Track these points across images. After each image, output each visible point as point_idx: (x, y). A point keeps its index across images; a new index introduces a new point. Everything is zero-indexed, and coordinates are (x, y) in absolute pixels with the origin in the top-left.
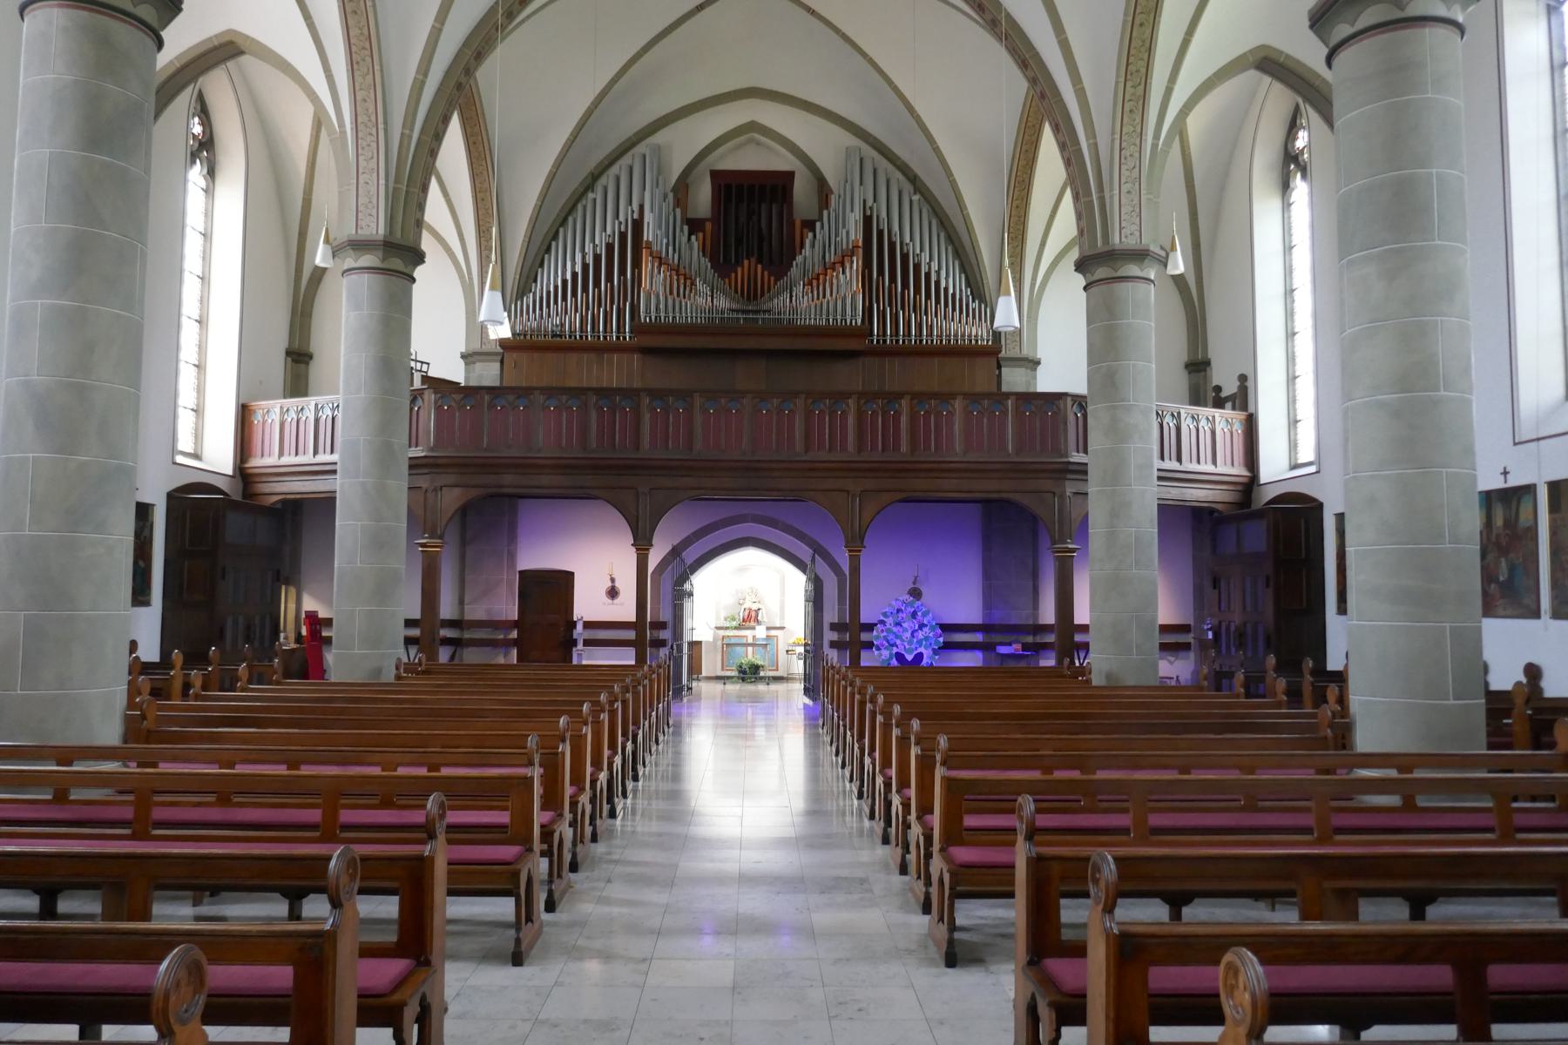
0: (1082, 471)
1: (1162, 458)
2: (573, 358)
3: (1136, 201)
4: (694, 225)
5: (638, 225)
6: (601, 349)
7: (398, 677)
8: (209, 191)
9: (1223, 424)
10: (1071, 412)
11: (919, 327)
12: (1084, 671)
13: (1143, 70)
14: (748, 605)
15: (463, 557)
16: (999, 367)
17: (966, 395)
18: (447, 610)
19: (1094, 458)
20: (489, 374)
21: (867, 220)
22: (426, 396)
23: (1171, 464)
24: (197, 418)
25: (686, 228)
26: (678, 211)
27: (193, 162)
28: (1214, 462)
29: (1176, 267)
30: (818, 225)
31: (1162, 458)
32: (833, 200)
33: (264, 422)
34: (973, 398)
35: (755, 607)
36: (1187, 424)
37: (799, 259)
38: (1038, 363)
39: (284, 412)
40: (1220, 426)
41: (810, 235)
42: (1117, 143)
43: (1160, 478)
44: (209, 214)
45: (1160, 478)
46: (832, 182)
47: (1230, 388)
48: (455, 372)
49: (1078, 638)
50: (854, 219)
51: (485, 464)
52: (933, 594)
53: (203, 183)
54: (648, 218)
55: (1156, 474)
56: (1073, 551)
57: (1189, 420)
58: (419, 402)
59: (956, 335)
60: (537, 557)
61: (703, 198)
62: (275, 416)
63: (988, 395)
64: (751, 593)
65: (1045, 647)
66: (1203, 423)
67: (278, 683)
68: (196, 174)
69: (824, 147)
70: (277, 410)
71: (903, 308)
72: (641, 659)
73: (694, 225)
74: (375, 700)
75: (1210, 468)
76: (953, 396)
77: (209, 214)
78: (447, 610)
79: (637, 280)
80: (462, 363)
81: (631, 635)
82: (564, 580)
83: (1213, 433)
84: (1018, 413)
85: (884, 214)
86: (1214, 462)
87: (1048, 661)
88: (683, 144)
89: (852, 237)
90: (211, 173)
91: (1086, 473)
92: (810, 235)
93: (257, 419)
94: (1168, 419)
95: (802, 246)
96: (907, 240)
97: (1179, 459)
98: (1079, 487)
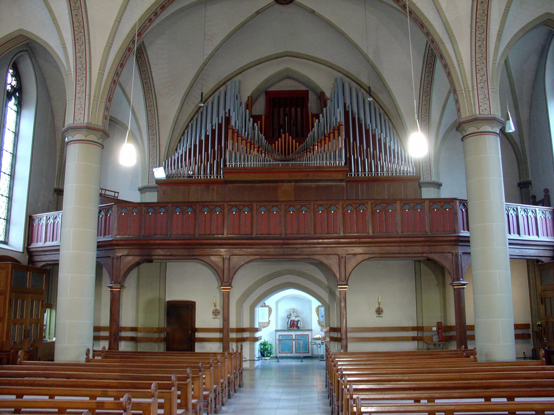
0: (466, 241)
1: (510, 233)
2: (193, 188)
3: (486, 92)
4: (256, 118)
5: (228, 120)
6: (208, 184)
7: (88, 360)
8: (19, 113)
9: (541, 214)
10: (460, 208)
11: (376, 167)
12: (473, 352)
13: (485, 26)
14: (293, 318)
15: (138, 295)
16: (420, 187)
17: (401, 200)
18: (233, 324)
19: (474, 233)
20: (152, 197)
21: (346, 113)
22: (113, 209)
23: (515, 236)
24: (7, 223)
25: (251, 119)
26: (247, 111)
27: (10, 99)
28: (537, 234)
29: (511, 129)
30: (321, 115)
31: (510, 233)
32: (329, 102)
33: (39, 224)
34: (405, 202)
35: (297, 319)
36: (521, 213)
37: (311, 133)
38: (441, 185)
39: (48, 219)
40: (539, 215)
41: (317, 120)
42: (474, 62)
43: (510, 244)
44: (18, 124)
45: (510, 244)
46: (328, 94)
47: (540, 196)
48: (135, 197)
49: (469, 333)
50: (340, 112)
51: (137, 239)
52: (383, 304)
53: (15, 108)
54: (233, 115)
55: (508, 241)
56: (464, 285)
57: (523, 212)
58: (110, 212)
59: (396, 171)
60: (177, 293)
61: (260, 108)
62: (44, 221)
63: (413, 200)
64: (284, 310)
65: (451, 338)
66: (530, 213)
67: (21, 364)
68: (12, 104)
69: (323, 81)
70: (45, 218)
71: (367, 157)
72: (226, 348)
73: (256, 118)
74: (143, 367)
75: (535, 238)
76: (394, 201)
77: (18, 124)
78: (233, 324)
79: (226, 146)
80: (139, 192)
81: (217, 335)
82: (190, 307)
83: (536, 219)
84: (431, 210)
85: (355, 110)
86: (538, 235)
87: (453, 346)
88: (252, 83)
89: (339, 120)
90: (20, 105)
91: (469, 241)
92: (317, 120)
93: (36, 223)
94: (511, 212)
95: (313, 127)
96: (368, 122)
97: (519, 233)
98: (466, 250)
